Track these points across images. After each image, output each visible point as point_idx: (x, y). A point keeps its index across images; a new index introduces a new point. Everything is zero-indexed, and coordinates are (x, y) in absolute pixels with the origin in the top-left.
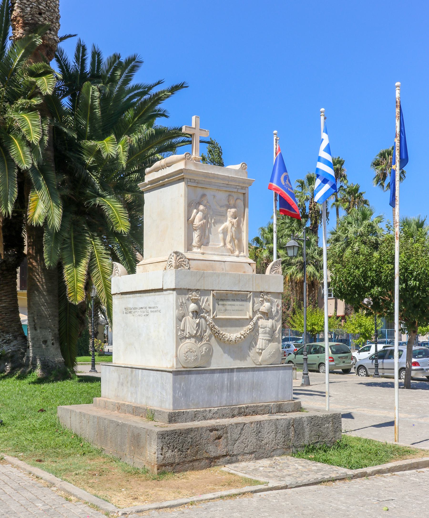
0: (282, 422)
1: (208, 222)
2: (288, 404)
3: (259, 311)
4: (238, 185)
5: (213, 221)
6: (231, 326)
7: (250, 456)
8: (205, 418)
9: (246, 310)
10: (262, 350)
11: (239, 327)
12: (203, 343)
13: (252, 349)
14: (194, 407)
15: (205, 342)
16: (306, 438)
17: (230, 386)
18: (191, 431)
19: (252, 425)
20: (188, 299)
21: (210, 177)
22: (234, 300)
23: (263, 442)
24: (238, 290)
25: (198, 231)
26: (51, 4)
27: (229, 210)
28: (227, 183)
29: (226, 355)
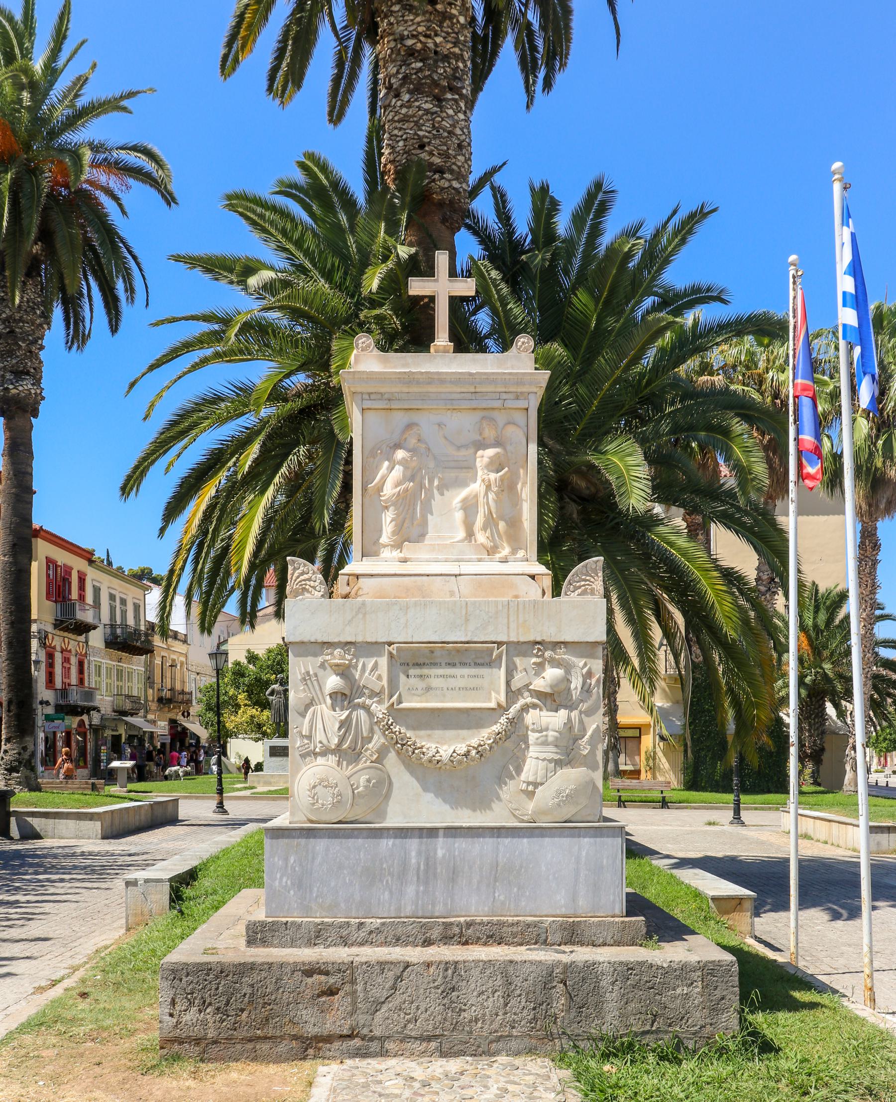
0: (527, 969)
1: (421, 486)
2: (600, 924)
3: (529, 691)
4: (503, 390)
5: (436, 483)
6: (446, 727)
7: (425, 1044)
8: (345, 942)
10: (536, 785)
11: (469, 728)
12: (360, 766)
13: (506, 784)
14: (324, 914)
15: (368, 763)
16: (608, 1018)
17: (427, 871)
18: (252, 969)
19: (432, 970)
20: (322, 666)
21: (418, 383)
22: (452, 665)
24: (463, 640)
25: (392, 508)
26: (444, 123)
27: (480, 453)
28: (473, 390)
29: (430, 796)
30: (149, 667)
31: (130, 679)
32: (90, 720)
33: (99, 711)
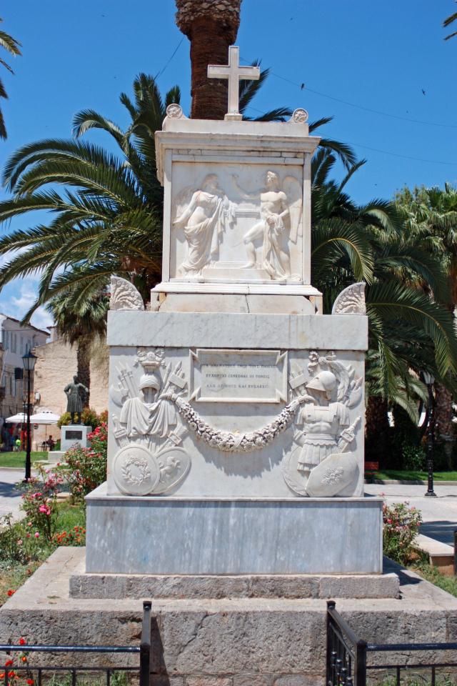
9: (269, 385)
10: (311, 466)
15: (173, 447)
23: (253, 656)
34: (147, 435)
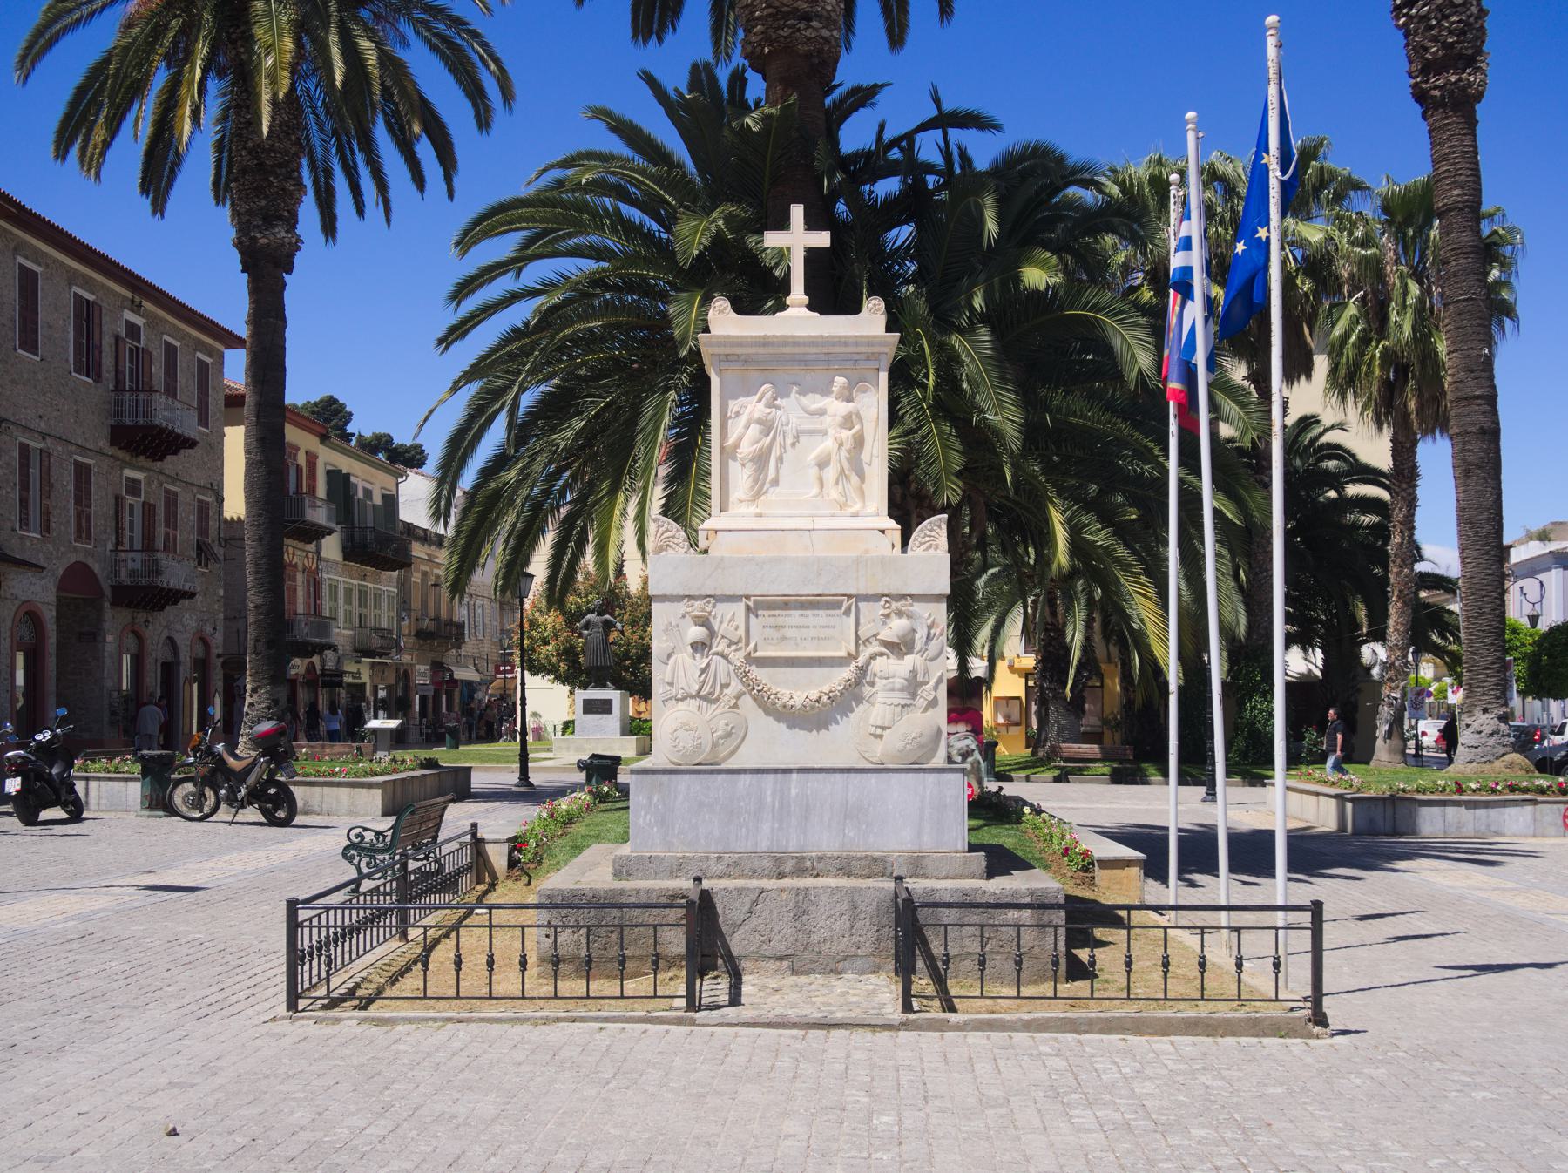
9: (832, 635)
10: (884, 728)
30: (403, 585)
31: (377, 605)
32: (323, 662)
33: (335, 650)
34: (698, 696)
